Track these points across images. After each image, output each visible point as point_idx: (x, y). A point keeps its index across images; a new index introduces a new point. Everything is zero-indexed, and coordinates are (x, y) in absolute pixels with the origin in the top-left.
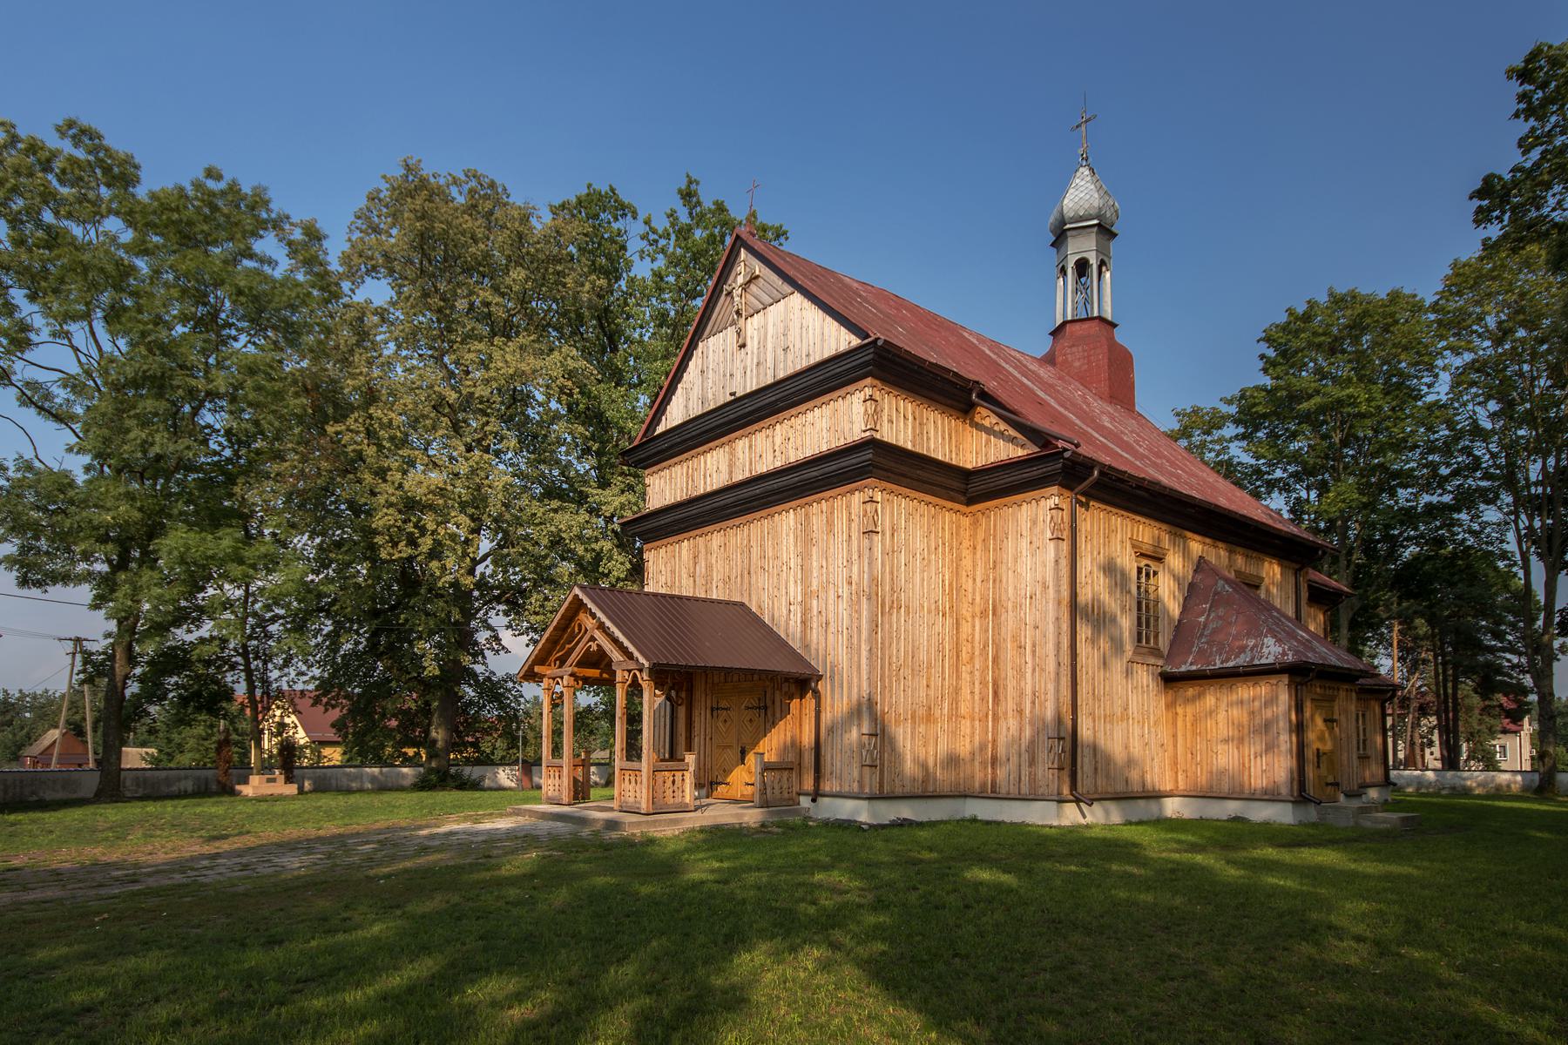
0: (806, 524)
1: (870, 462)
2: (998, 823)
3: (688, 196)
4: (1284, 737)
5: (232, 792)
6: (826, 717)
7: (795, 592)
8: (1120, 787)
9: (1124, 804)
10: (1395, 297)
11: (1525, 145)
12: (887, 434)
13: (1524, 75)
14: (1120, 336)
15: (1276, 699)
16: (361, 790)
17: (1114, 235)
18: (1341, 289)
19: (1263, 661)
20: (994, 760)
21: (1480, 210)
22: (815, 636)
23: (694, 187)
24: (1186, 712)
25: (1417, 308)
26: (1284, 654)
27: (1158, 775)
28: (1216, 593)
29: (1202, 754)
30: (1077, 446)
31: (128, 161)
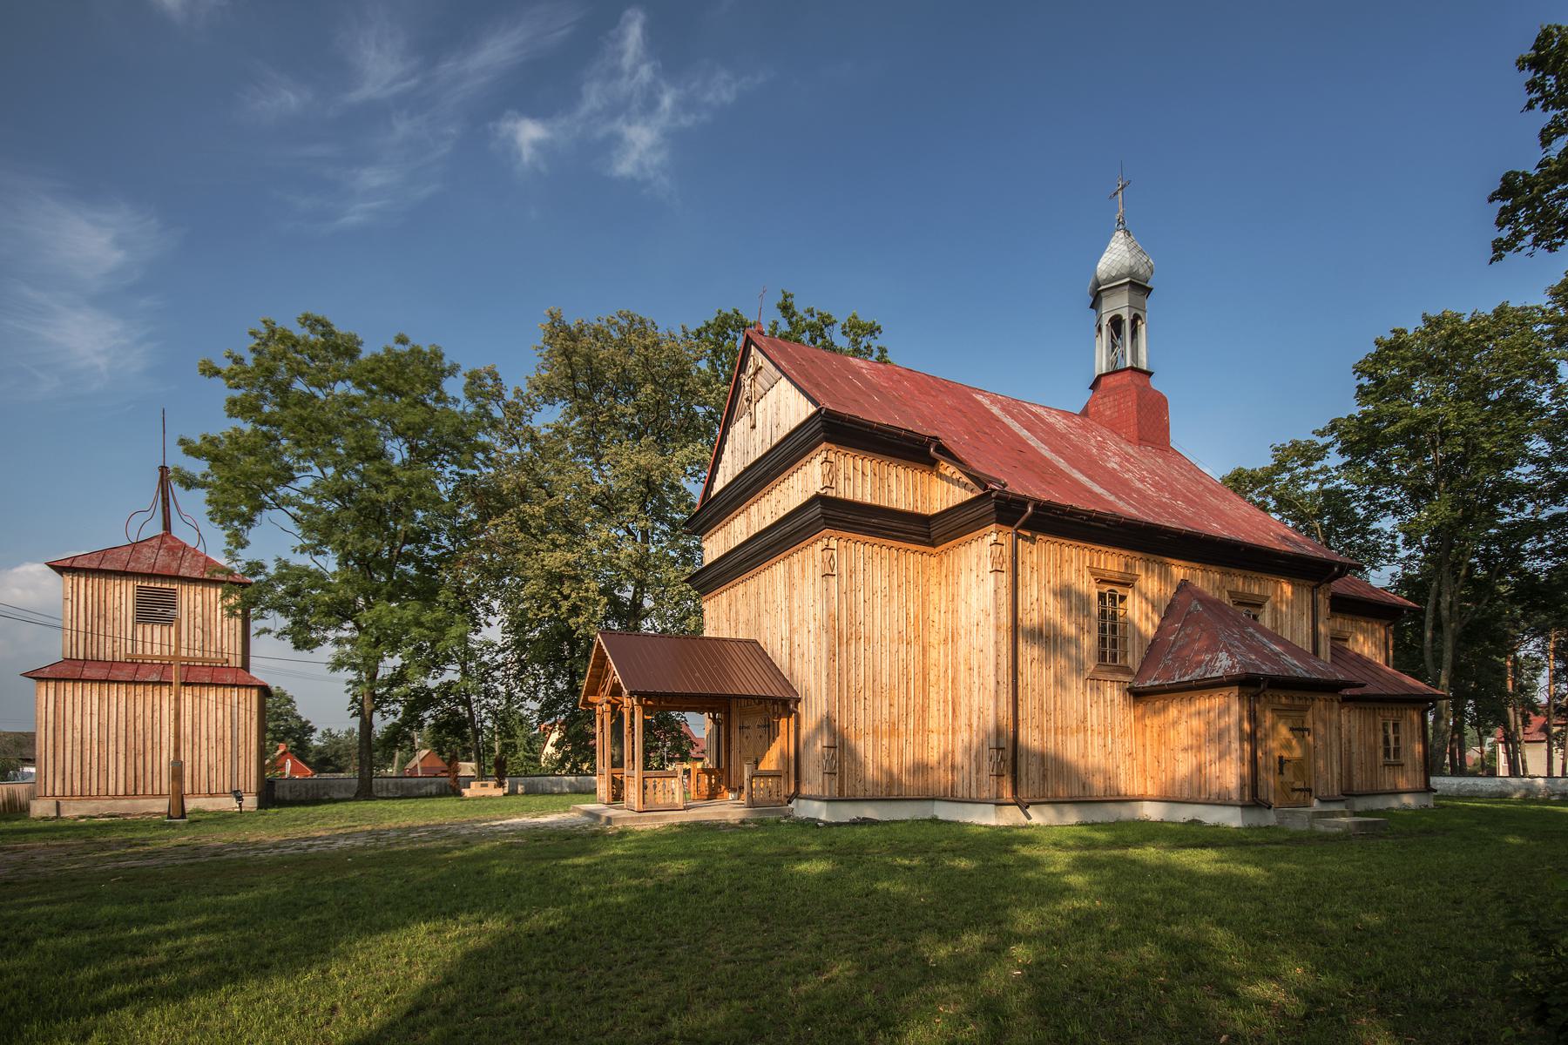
0: (790, 571)
1: (833, 514)
2: (957, 823)
3: (786, 309)
4: (1235, 745)
5: (460, 794)
6: (803, 732)
7: (785, 628)
8: (1076, 791)
9: (1085, 807)
10: (1500, 312)
11: (1546, 138)
12: (845, 491)
13: (1536, 63)
14: (1155, 383)
15: (1226, 709)
16: (560, 794)
17: (1150, 290)
18: (1434, 313)
19: (1215, 674)
20: (953, 767)
21: (1504, 210)
22: (797, 665)
23: (789, 300)
24: (1153, 722)
25: (1524, 318)
26: (1233, 667)
27: (1129, 783)
28: (1189, 613)
29: (1165, 759)
30: (1005, 485)
31: (353, 338)
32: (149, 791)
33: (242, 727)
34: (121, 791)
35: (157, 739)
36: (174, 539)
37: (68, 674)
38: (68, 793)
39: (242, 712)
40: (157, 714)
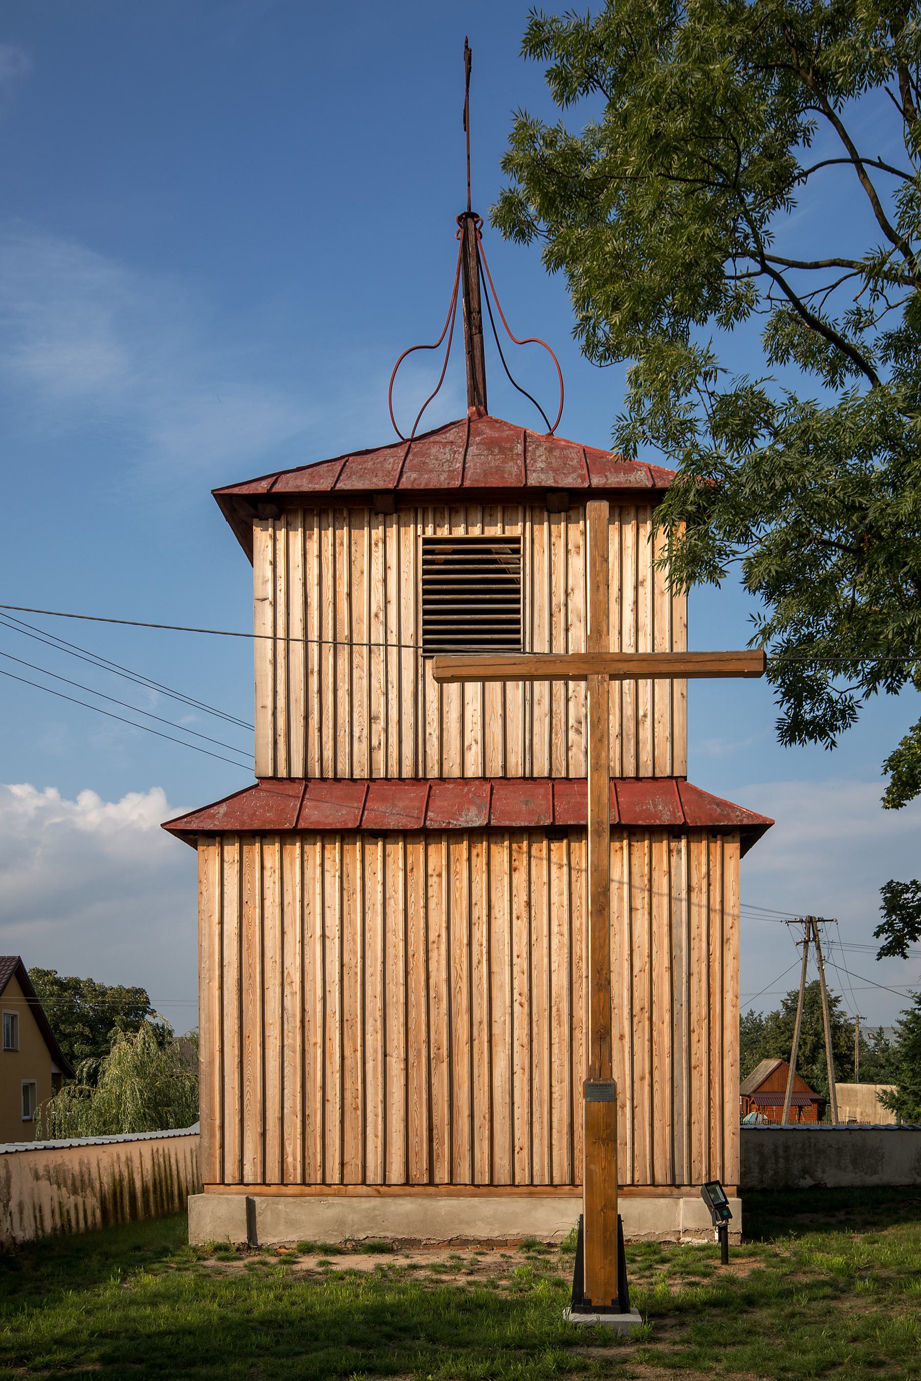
32: (464, 1176)
33: (699, 968)
34: (396, 1175)
35: (480, 1013)
36: (496, 423)
37: (268, 819)
38: (273, 1175)
39: (699, 917)
40: (480, 934)
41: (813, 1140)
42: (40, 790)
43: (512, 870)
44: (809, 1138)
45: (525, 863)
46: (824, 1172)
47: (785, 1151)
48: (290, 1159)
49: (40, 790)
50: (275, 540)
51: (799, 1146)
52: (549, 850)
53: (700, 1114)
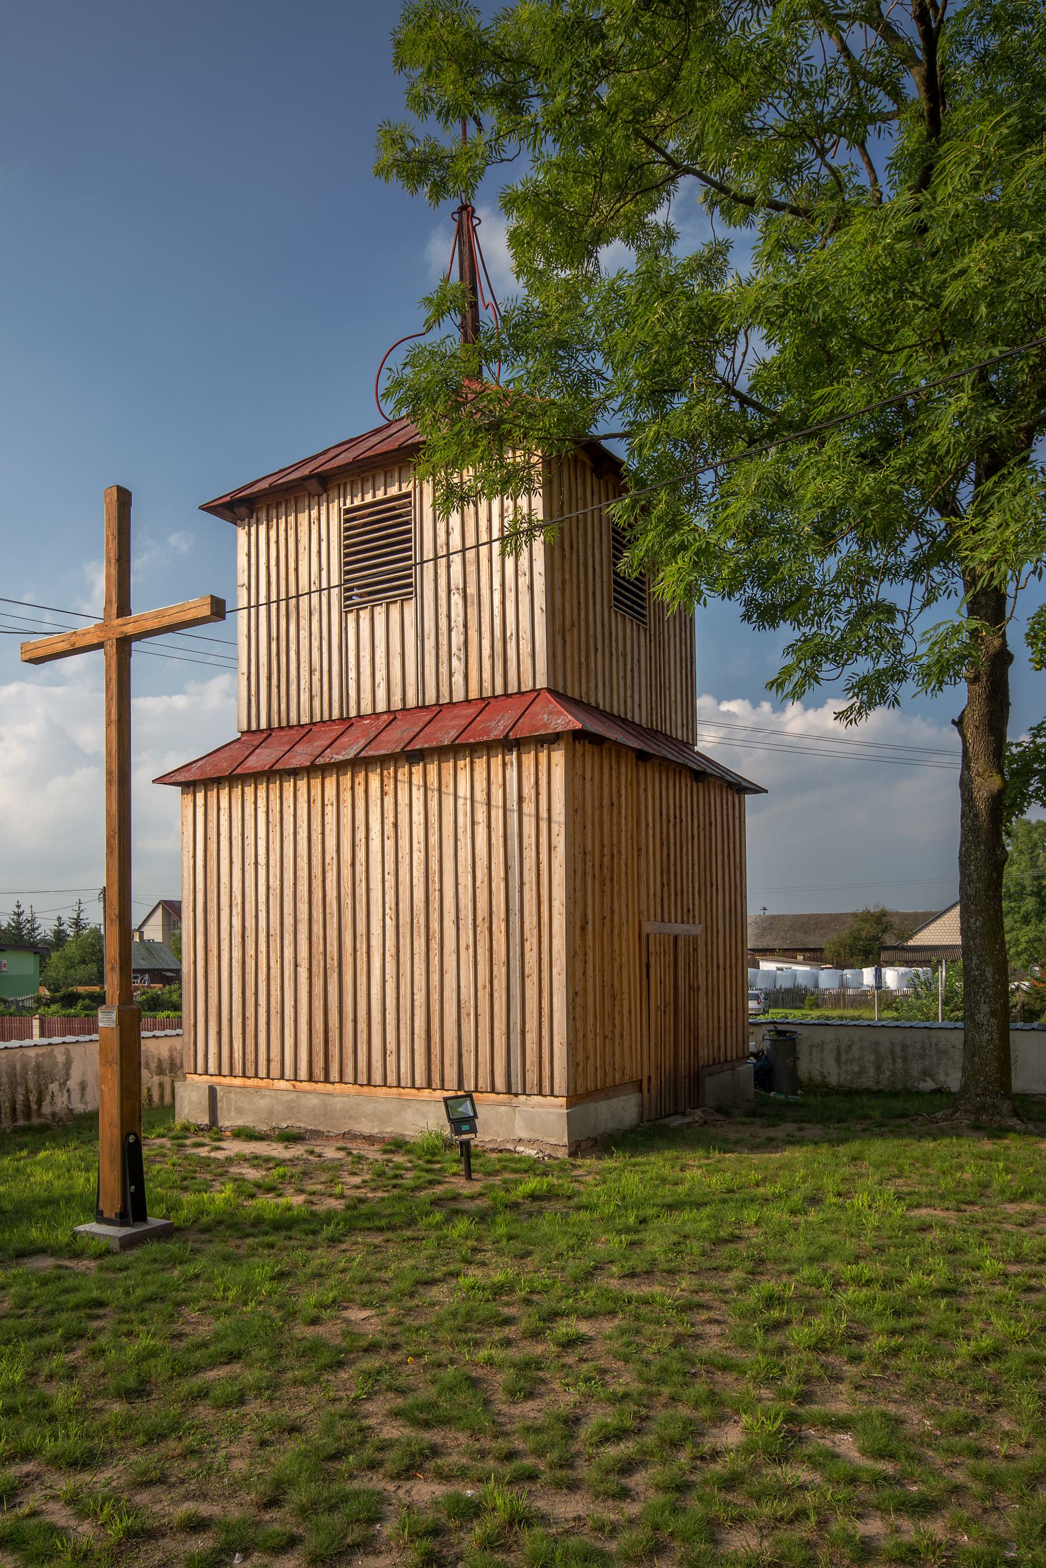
33: (530, 877)
41: (934, 1040)
42: (755, 704)
43: (383, 794)
44: (929, 1037)
45: (392, 787)
46: (947, 1075)
47: (903, 1050)
48: (236, 1055)
49: (755, 704)
50: (249, 534)
51: (918, 1045)
52: (411, 773)
53: (532, 1024)
